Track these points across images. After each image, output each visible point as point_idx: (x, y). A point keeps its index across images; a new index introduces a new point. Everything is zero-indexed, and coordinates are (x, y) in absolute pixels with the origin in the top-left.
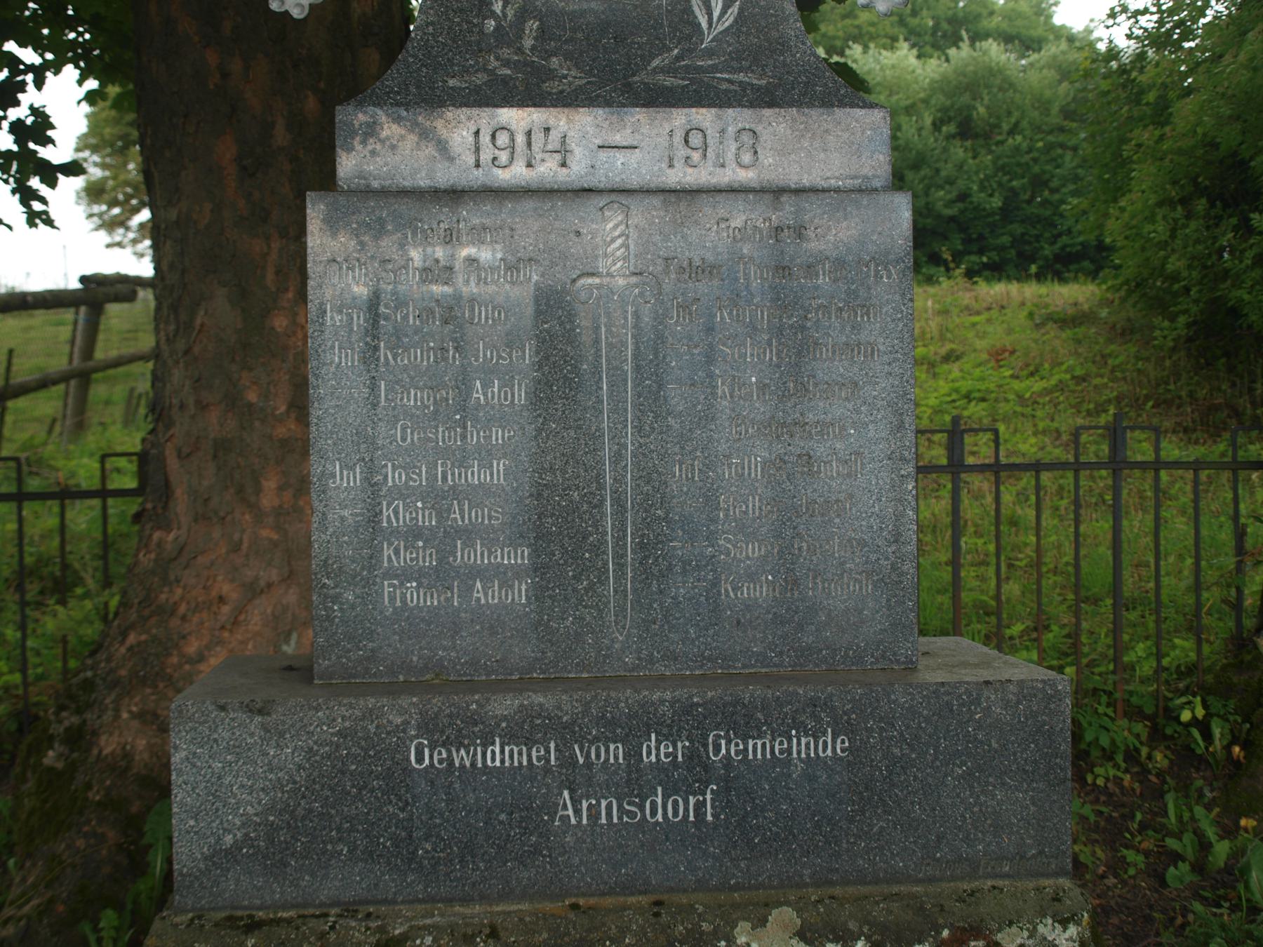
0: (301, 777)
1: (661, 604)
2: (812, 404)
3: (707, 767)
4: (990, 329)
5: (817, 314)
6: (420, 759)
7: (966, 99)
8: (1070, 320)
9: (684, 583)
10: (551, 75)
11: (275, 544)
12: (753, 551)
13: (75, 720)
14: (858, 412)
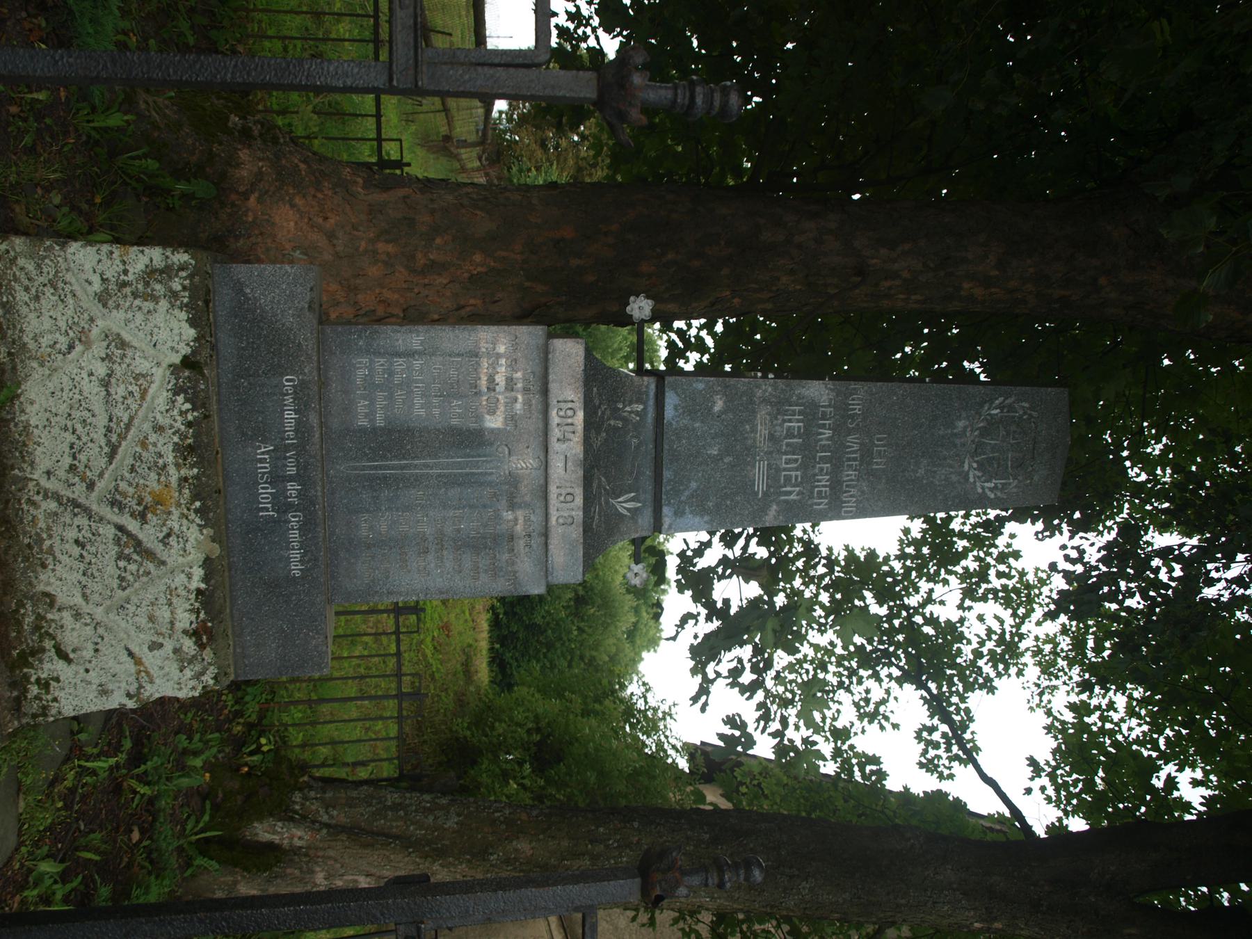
0: (278, 325)
3: (285, 512)
4: (461, 622)
6: (287, 380)
7: (599, 601)
8: (468, 670)
10: (598, 433)
11: (357, 249)
12: (384, 528)
13: (256, 133)
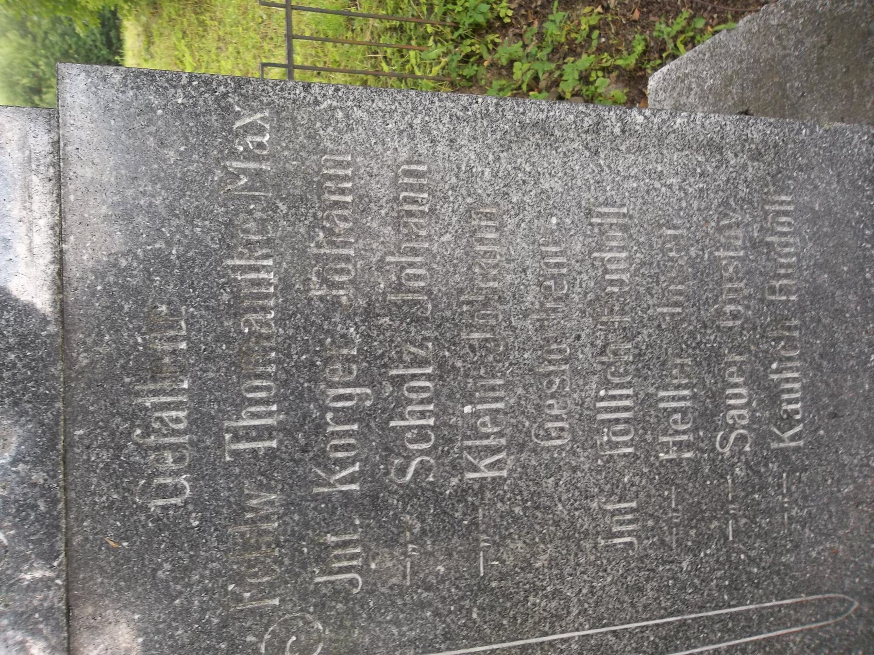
1: (812, 545)
2: (508, 295)
5: (340, 285)
7: (19, 89)
9: (783, 510)
14: (520, 207)
